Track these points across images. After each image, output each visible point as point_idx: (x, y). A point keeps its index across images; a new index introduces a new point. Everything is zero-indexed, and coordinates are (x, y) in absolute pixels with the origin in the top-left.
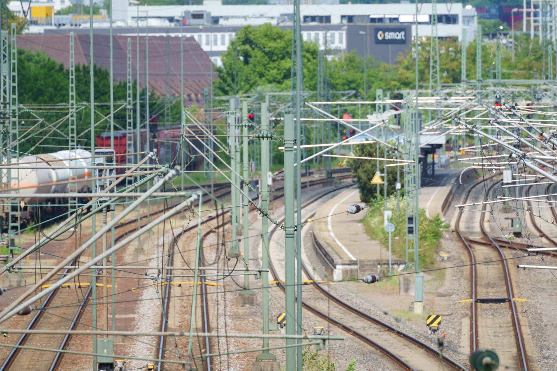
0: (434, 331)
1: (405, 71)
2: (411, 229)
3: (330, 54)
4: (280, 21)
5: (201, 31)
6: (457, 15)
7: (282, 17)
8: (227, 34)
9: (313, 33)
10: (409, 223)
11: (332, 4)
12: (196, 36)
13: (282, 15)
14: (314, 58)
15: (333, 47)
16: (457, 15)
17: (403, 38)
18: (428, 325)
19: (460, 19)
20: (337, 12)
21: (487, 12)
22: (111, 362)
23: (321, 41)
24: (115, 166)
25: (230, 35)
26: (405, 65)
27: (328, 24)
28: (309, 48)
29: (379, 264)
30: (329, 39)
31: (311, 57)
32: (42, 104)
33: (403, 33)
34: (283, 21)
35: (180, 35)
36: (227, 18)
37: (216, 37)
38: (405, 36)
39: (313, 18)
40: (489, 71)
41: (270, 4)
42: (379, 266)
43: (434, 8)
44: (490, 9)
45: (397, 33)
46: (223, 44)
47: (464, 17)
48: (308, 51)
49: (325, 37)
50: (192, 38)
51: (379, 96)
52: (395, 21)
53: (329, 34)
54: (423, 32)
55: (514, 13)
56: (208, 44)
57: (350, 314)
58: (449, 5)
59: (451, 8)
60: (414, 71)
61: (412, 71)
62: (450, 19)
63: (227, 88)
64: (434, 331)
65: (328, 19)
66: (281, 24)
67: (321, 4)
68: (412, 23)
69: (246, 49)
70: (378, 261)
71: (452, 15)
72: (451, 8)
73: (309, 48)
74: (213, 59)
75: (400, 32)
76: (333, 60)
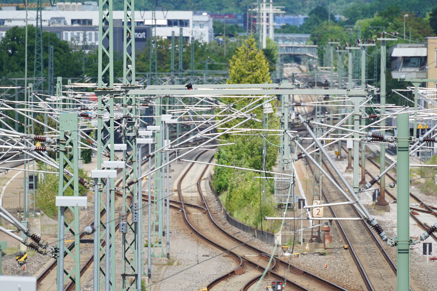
0: (21, 264)
2: (31, 186)
4: (51, 23)
6: (188, 20)
7: (52, 20)
9: (75, 33)
10: (30, 181)
11: (93, 10)
13: (52, 19)
14: (65, 52)
15: (89, 43)
16: (188, 20)
17: (144, 37)
18: (17, 260)
19: (191, 23)
20: (95, 15)
21: (235, 18)
22: (424, 55)
23: (81, 38)
26: (141, 58)
27: (90, 26)
28: (61, 44)
29: (18, 212)
33: (144, 33)
34: (52, 24)
36: (10, 20)
38: (146, 35)
39: (79, 21)
40: (205, 63)
41: (46, 10)
42: (18, 214)
43: (154, 15)
44: (237, 15)
45: (140, 34)
47: (193, 21)
49: (85, 35)
51: (59, 82)
52: (141, 24)
53: (87, 33)
54: (163, 33)
55: (406, 17)
57: (226, 246)
58: (165, 12)
59: (143, 15)
60: (149, 63)
61: (147, 62)
62: (183, 23)
64: (21, 264)
65: (90, 22)
66: (51, 26)
67: (85, 10)
68: (153, 26)
69: (14, 44)
70: (17, 209)
71: (184, 20)
72: (143, 15)
73: (61, 44)
75: (141, 33)
76: (89, 53)
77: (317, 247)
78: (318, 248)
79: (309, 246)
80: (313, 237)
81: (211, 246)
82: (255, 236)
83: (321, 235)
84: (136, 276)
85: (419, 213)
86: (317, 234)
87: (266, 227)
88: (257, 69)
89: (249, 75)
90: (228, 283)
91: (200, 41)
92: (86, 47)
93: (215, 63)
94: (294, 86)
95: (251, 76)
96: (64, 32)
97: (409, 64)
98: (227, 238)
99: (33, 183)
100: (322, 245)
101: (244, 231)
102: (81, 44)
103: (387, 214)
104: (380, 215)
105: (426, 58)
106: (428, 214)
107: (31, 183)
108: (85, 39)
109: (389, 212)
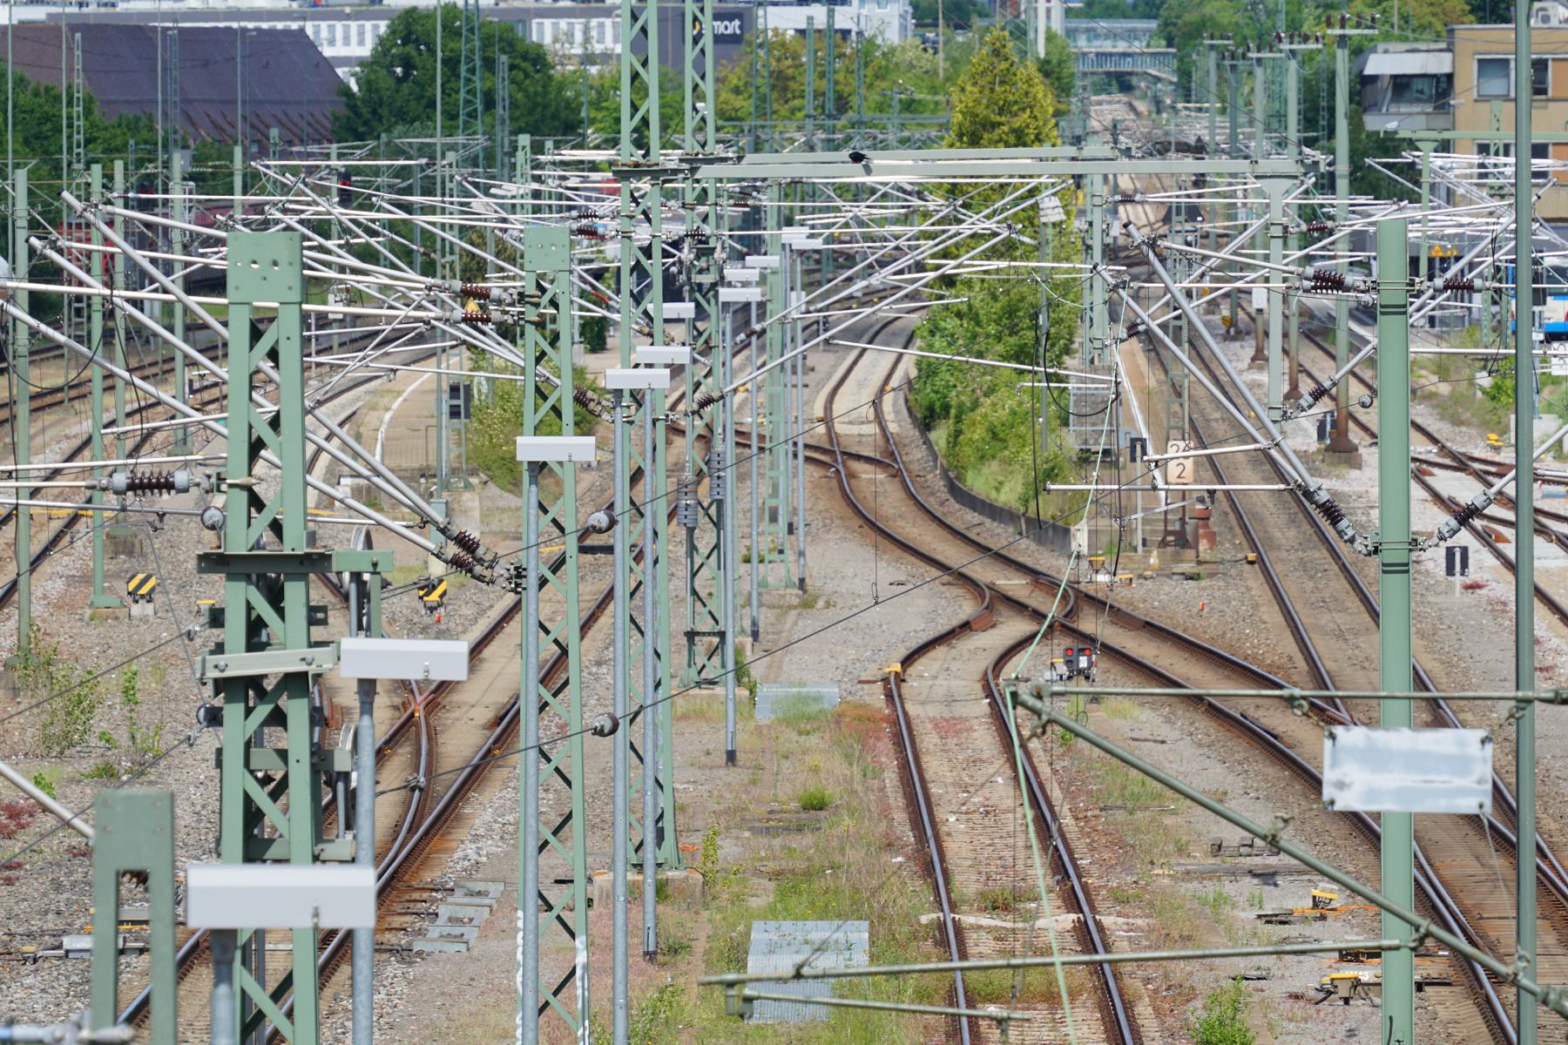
0: (432, 609)
1: (731, 97)
3: (594, 63)
5: (348, 17)
8: (368, 25)
9: (563, 24)
10: (452, 397)
12: (309, 28)
15: (598, 48)
22: (1447, 69)
24: (655, 267)
25: (376, 27)
28: (527, 52)
30: (594, 33)
31: (530, 68)
32: (334, 148)
33: (737, 23)
35: (235, 25)
37: (347, 29)
38: (741, 27)
42: (423, 480)
46: (361, 42)
48: (525, 57)
50: (302, 30)
53: (594, 22)
56: (332, 42)
63: (361, 129)
64: (432, 609)
74: (340, 71)
77: (1178, 559)
78: (1182, 561)
79: (1159, 556)
80: (1168, 533)
81: (912, 559)
82: (1020, 533)
83: (1189, 529)
84: (722, 635)
85: (1435, 470)
86: (1177, 527)
87: (1048, 509)
88: (1024, 110)
89: (1000, 124)
90: (953, 652)
91: (879, 41)
92: (588, 59)
93: (918, 96)
94: (1117, 153)
95: (1006, 129)
96: (535, 21)
97: (1407, 95)
98: (950, 537)
99: (461, 402)
100: (1190, 553)
101: (994, 520)
102: (578, 51)
103: (1354, 473)
104: (1338, 477)
105: (1450, 77)
106: (1459, 474)
107: (455, 402)
108: (587, 40)
109: (1360, 468)
